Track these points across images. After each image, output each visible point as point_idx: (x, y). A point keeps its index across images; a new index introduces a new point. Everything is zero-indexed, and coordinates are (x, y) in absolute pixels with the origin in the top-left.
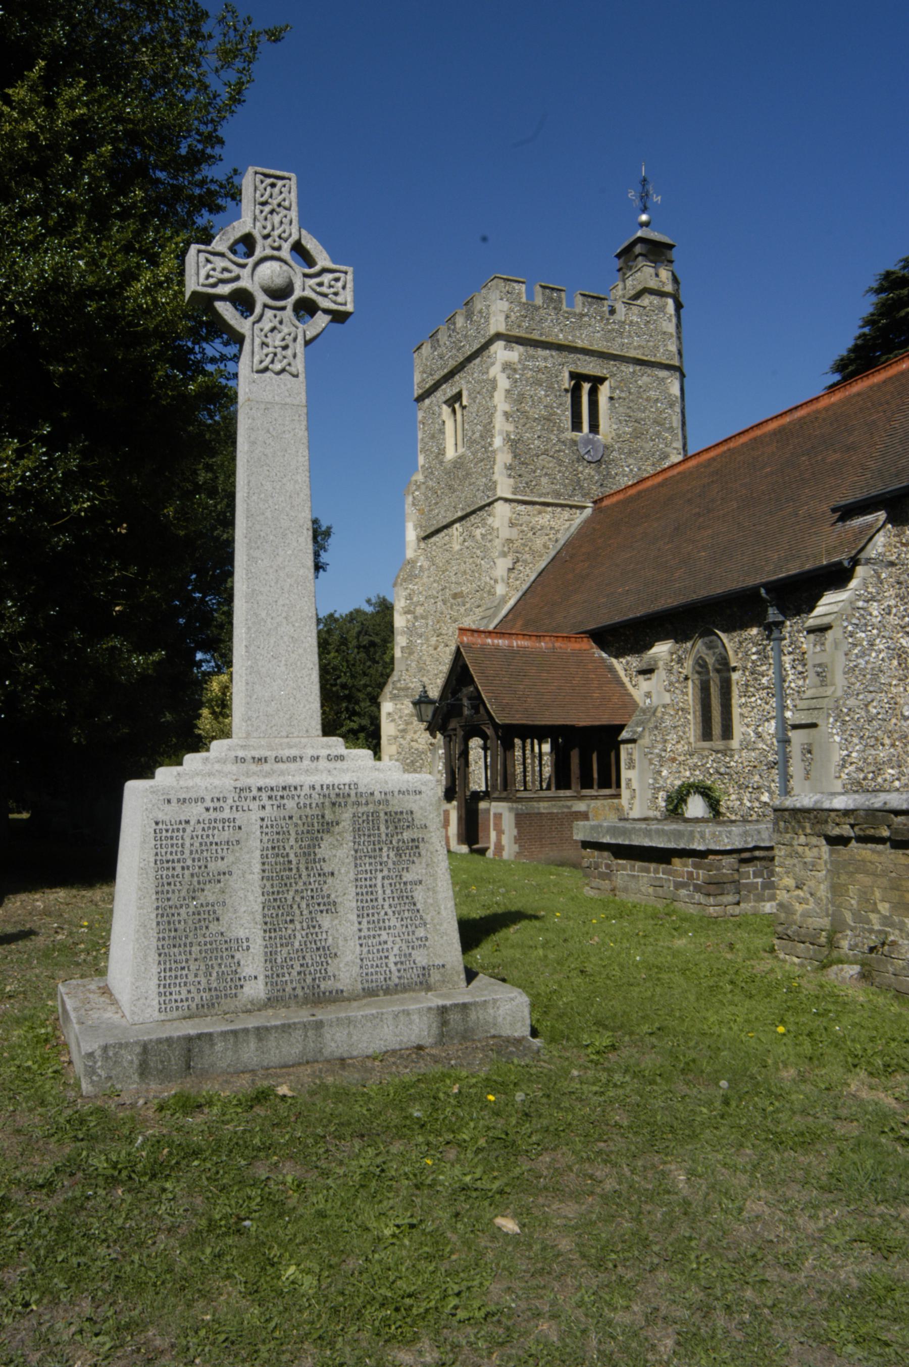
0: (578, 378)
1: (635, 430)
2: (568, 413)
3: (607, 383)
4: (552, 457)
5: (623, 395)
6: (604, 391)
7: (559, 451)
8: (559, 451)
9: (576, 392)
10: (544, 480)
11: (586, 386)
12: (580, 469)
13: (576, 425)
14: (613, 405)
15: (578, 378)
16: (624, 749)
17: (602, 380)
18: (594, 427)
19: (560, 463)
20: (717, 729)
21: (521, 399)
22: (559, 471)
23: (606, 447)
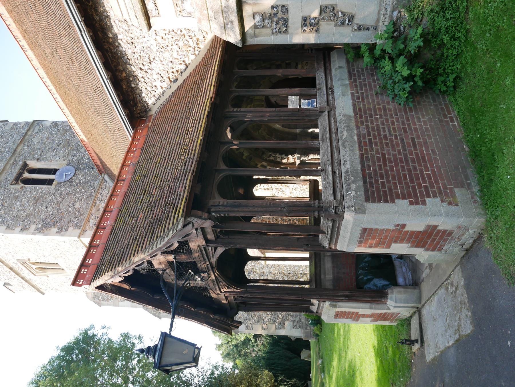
0: (19, 179)
1: (64, 147)
2: (38, 187)
3: (28, 162)
4: (64, 198)
5: (39, 153)
6: (33, 164)
7: (61, 194)
8: (61, 194)
9: (27, 181)
10: (77, 205)
11: (26, 175)
12: (77, 181)
13: (50, 182)
14: (43, 159)
15: (19, 179)
16: (251, 41)
17: (25, 165)
18: (54, 171)
19: (69, 193)
20: (219, 39)
21: (16, 218)
22: (75, 195)
23: (68, 165)
